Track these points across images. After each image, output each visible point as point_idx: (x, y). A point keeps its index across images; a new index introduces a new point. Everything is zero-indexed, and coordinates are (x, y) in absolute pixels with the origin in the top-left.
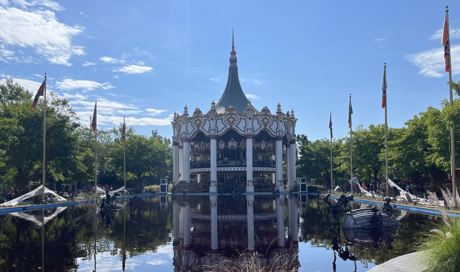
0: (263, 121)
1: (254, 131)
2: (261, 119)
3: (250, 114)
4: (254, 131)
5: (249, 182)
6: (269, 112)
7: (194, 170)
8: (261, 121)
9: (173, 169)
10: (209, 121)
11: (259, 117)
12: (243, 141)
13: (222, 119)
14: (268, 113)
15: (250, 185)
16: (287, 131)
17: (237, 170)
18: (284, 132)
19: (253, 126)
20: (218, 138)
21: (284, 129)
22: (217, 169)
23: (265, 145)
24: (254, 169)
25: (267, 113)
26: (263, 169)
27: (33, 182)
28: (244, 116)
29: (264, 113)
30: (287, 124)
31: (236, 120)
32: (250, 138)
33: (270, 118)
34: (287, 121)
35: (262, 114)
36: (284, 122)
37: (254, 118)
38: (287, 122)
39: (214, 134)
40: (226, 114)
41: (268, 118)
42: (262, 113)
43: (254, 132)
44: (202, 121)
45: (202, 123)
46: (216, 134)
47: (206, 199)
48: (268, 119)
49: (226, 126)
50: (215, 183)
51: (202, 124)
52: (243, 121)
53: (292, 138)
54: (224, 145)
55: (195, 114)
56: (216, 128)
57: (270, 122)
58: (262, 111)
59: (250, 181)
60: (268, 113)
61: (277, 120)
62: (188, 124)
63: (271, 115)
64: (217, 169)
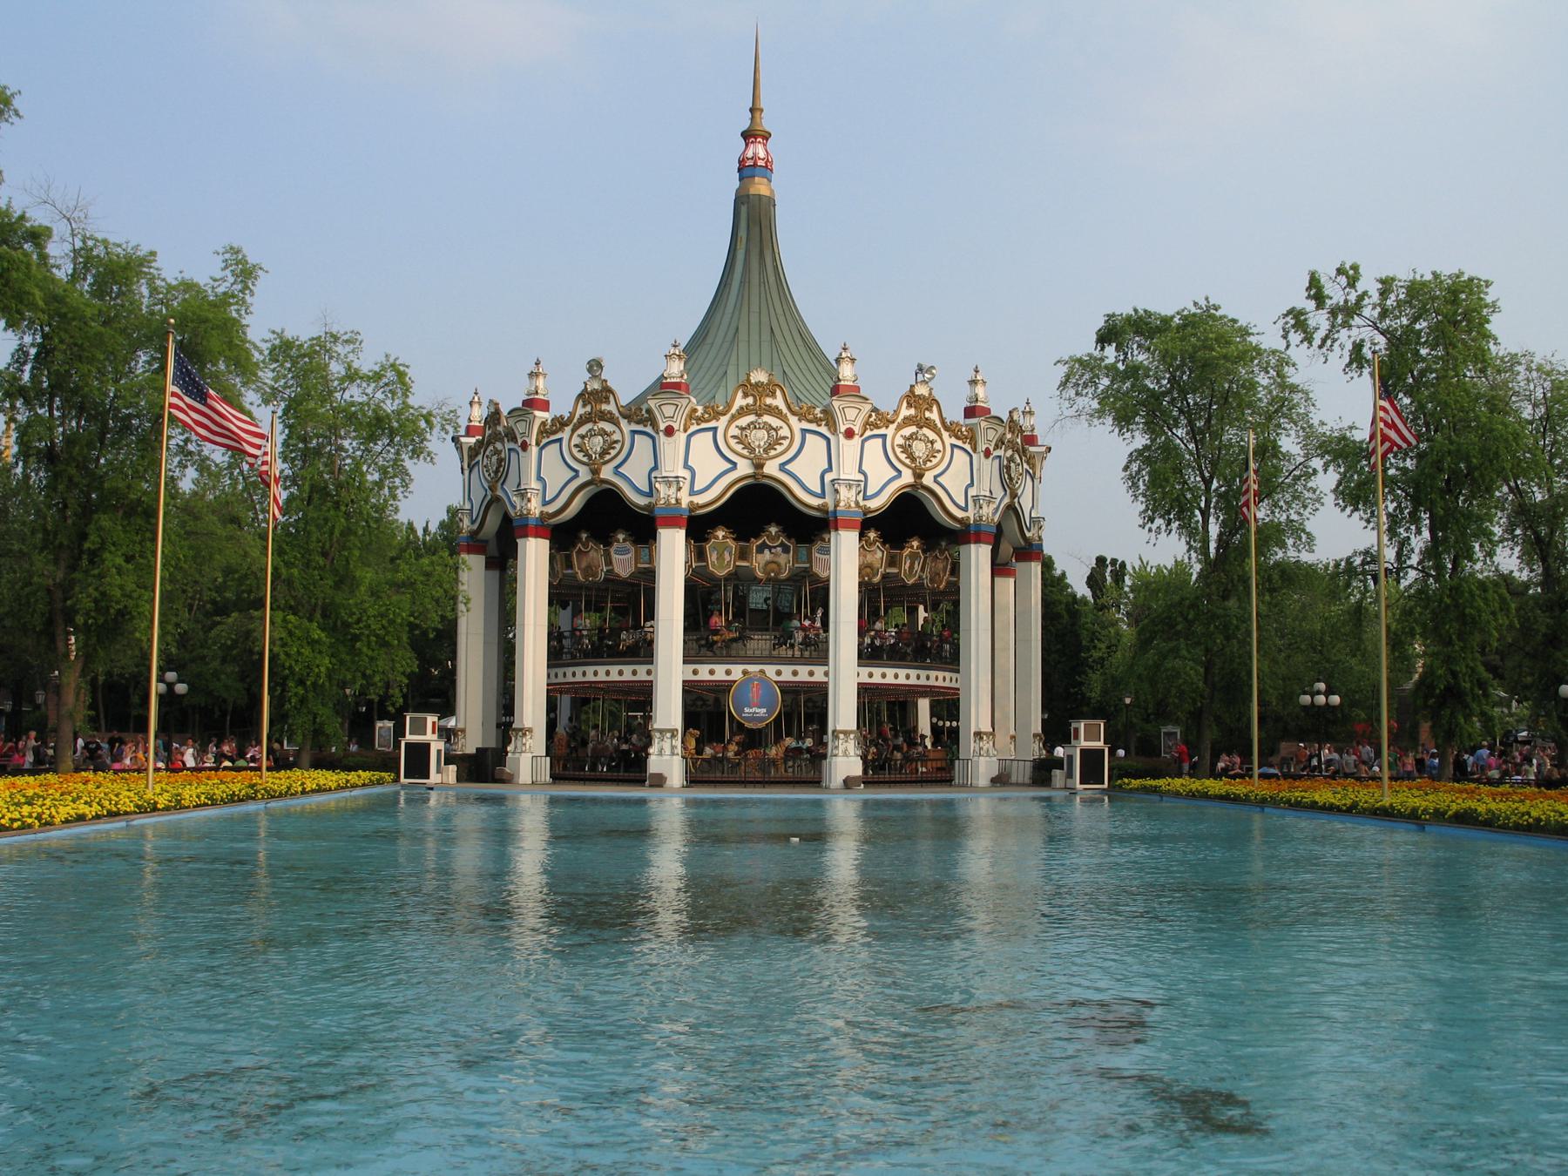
0: (906, 449)
1: (819, 491)
3: (851, 414)
5: (841, 736)
7: (941, 678)
8: (900, 446)
13: (884, 437)
14: (931, 411)
15: (846, 754)
16: (1007, 500)
18: (997, 501)
20: (698, 527)
21: (999, 493)
23: (631, 555)
24: (649, 672)
29: (912, 411)
30: (1008, 468)
31: (784, 438)
34: (1009, 453)
36: (1000, 457)
37: (868, 433)
38: (1011, 459)
40: (733, 411)
42: (905, 412)
43: (865, 499)
44: (938, 446)
48: (932, 442)
50: (673, 736)
51: (935, 461)
52: (815, 445)
53: (1028, 534)
55: (584, 406)
56: (687, 474)
59: (846, 733)
62: (866, 444)
64: (826, 674)
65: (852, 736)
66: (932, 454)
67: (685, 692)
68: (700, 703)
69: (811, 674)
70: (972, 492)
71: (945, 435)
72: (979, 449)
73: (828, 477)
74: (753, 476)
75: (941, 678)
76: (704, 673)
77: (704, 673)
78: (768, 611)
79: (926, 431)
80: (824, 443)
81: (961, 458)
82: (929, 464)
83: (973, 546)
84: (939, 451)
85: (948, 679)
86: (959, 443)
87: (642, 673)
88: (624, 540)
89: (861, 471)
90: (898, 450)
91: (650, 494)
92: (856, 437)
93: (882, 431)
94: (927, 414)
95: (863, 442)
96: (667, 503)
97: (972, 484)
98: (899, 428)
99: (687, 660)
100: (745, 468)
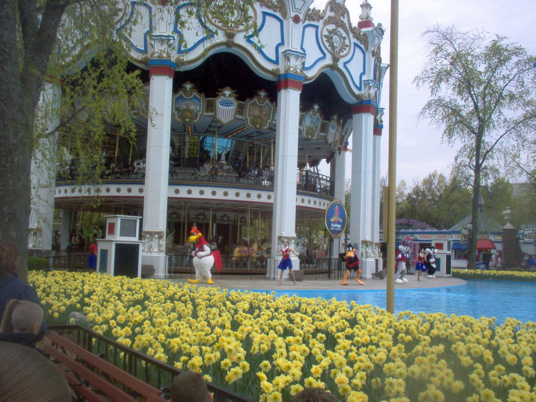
0: (329, 39)
1: (274, 59)
2: (325, 33)
4: (274, 59)
6: (346, 15)
8: (326, 36)
9: (296, 170)
10: (150, 8)
11: (320, 24)
12: (224, 95)
14: (344, 17)
17: (210, 196)
19: (302, 48)
22: (269, 197)
24: (141, 191)
25: (342, 18)
26: (237, 195)
27: (263, 171)
28: (276, 7)
29: (332, 14)
30: (329, 39)
32: (295, 86)
33: (348, 35)
34: (331, 27)
35: (330, 18)
37: (307, 22)
39: (299, 71)
41: (344, 35)
42: (329, 14)
45: (121, 14)
46: (174, 56)
47: (330, 260)
48: (344, 38)
49: (248, 39)
50: (160, 237)
51: (345, 52)
54: (233, 108)
57: (347, 49)
58: (329, 8)
60: (344, 17)
61: (278, 14)
62: (306, 30)
63: (350, 24)
65: (293, 241)
66: (344, 47)
67: (170, 207)
68: (201, 217)
69: (248, 195)
70: (364, 78)
71: (351, 35)
72: (369, 50)
73: (282, 49)
74: (226, 44)
75: (318, 203)
76: (183, 192)
77: (183, 192)
78: (237, 140)
79: (340, 30)
80: (278, 24)
81: (359, 54)
82: (341, 54)
83: (363, 114)
84: (347, 46)
85: (322, 204)
86: (358, 43)
87: (135, 191)
88: (230, 96)
89: (302, 48)
90: (325, 39)
91: (145, 51)
92: (301, 23)
93: (315, 23)
94: (342, 18)
95: (305, 27)
96: (160, 56)
97: (282, 43)
98: (325, 24)
99: (172, 182)
100: (220, 38)
